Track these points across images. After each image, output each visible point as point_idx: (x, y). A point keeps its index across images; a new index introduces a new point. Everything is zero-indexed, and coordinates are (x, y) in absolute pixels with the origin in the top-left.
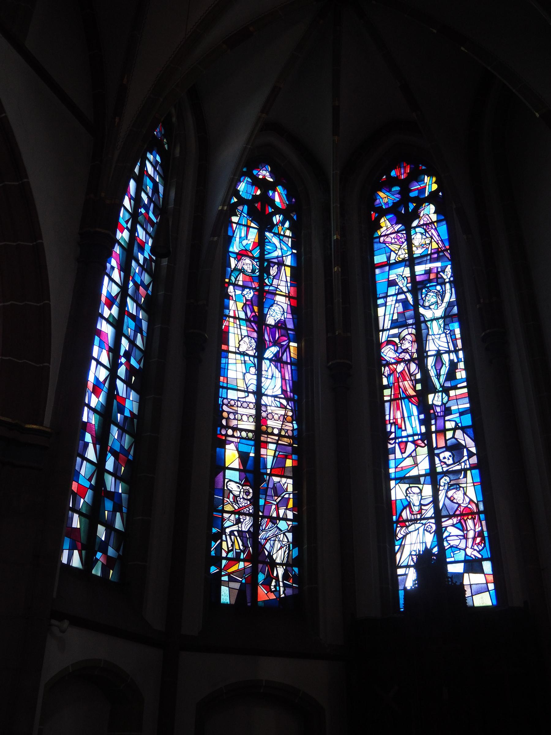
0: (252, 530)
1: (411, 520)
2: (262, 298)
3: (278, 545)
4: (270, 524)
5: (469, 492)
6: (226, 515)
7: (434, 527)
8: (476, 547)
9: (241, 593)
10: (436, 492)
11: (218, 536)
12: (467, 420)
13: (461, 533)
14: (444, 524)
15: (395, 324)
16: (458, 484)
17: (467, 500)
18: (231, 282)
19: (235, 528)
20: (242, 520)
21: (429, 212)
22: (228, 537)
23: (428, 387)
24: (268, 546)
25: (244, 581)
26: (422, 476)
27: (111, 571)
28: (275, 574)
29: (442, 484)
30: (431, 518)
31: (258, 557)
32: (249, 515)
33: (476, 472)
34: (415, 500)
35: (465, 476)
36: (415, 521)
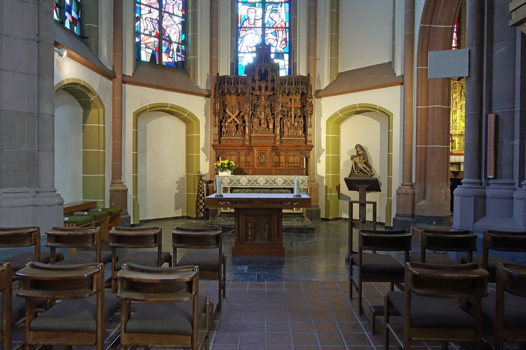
0: (158, 19)
1: (249, 28)
3: (173, 31)
4: (169, 17)
6: (142, 6)
7: (261, 33)
8: (282, 46)
9: (153, 56)
10: (264, 13)
11: (138, 19)
13: (275, 38)
14: (266, 32)
16: (277, 10)
17: (281, 20)
18: (266, 29)
19: (148, 16)
20: (152, 11)
22: (144, 21)
24: (168, 31)
25: (154, 49)
26: (257, 3)
27: (75, 28)
28: (172, 48)
29: (268, 9)
30: (260, 27)
31: (161, 35)
32: (156, 9)
33: (287, 5)
34: (252, 16)
35: (281, 6)
36: (251, 28)
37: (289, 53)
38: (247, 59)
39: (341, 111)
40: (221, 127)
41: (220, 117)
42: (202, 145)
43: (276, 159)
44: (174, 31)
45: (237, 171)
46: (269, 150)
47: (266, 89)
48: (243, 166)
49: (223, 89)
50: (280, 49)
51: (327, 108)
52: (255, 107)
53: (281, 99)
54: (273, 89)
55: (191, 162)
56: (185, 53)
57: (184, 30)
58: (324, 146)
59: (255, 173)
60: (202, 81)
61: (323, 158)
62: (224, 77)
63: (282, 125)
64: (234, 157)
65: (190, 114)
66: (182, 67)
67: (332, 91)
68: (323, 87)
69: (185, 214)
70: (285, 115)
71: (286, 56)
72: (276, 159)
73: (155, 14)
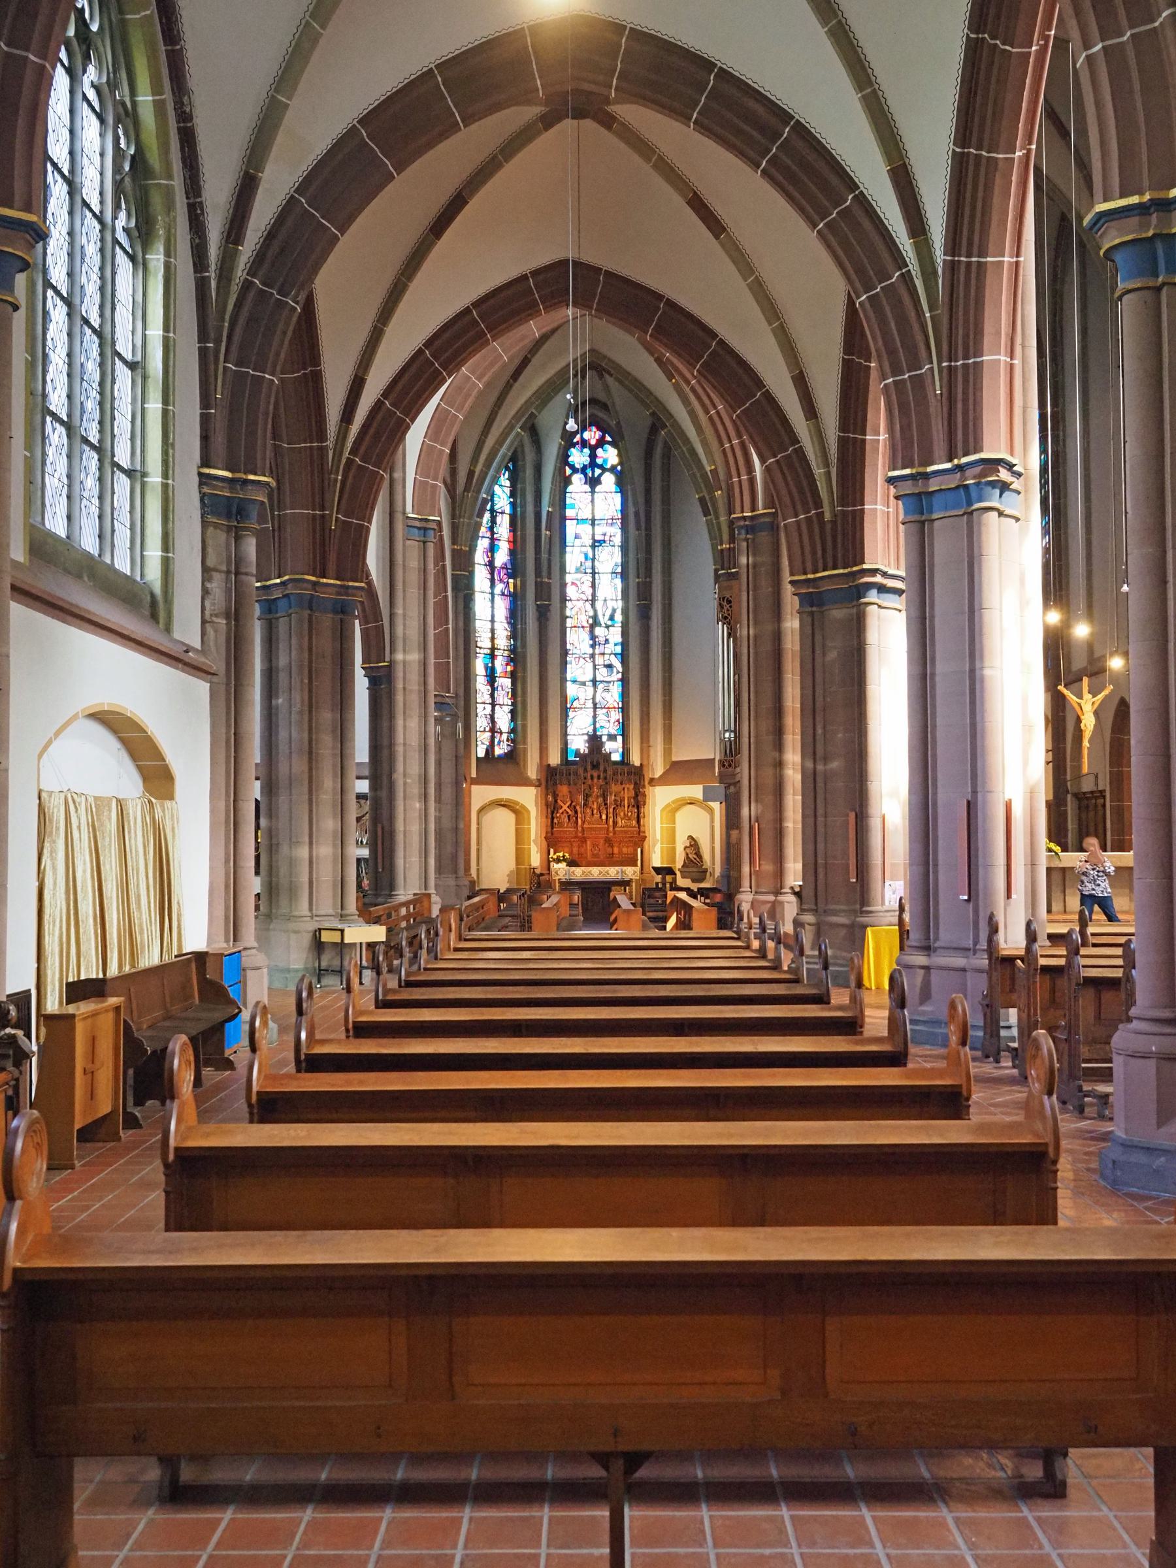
2: (492, 549)
5: (613, 695)
9: (487, 751)
12: (619, 649)
15: (578, 570)
21: (609, 480)
23: (595, 623)
37: (623, 735)
38: (578, 743)
39: (673, 802)
40: (553, 818)
41: (551, 809)
42: (533, 837)
43: (609, 850)
44: (504, 721)
45: (572, 863)
46: (602, 841)
47: (599, 777)
48: (576, 857)
49: (551, 778)
50: (613, 732)
51: (660, 798)
52: (586, 797)
53: (614, 788)
54: (605, 778)
55: (521, 855)
56: (513, 741)
57: (513, 719)
58: (658, 837)
59: (589, 864)
60: (532, 772)
61: (658, 848)
62: (555, 769)
63: (615, 815)
64: (567, 849)
65: (523, 807)
66: (512, 757)
67: (664, 780)
68: (657, 776)
69: (159, 1152)
70: (618, 804)
71: (620, 738)
72: (609, 850)
73: (489, 708)
